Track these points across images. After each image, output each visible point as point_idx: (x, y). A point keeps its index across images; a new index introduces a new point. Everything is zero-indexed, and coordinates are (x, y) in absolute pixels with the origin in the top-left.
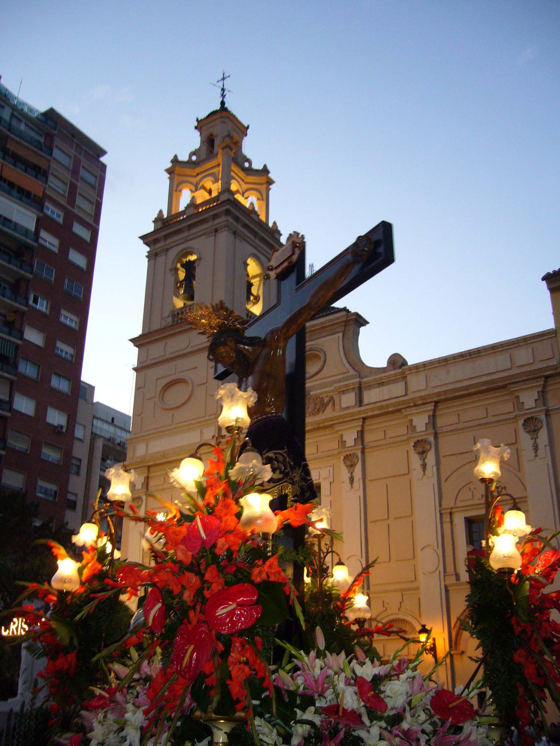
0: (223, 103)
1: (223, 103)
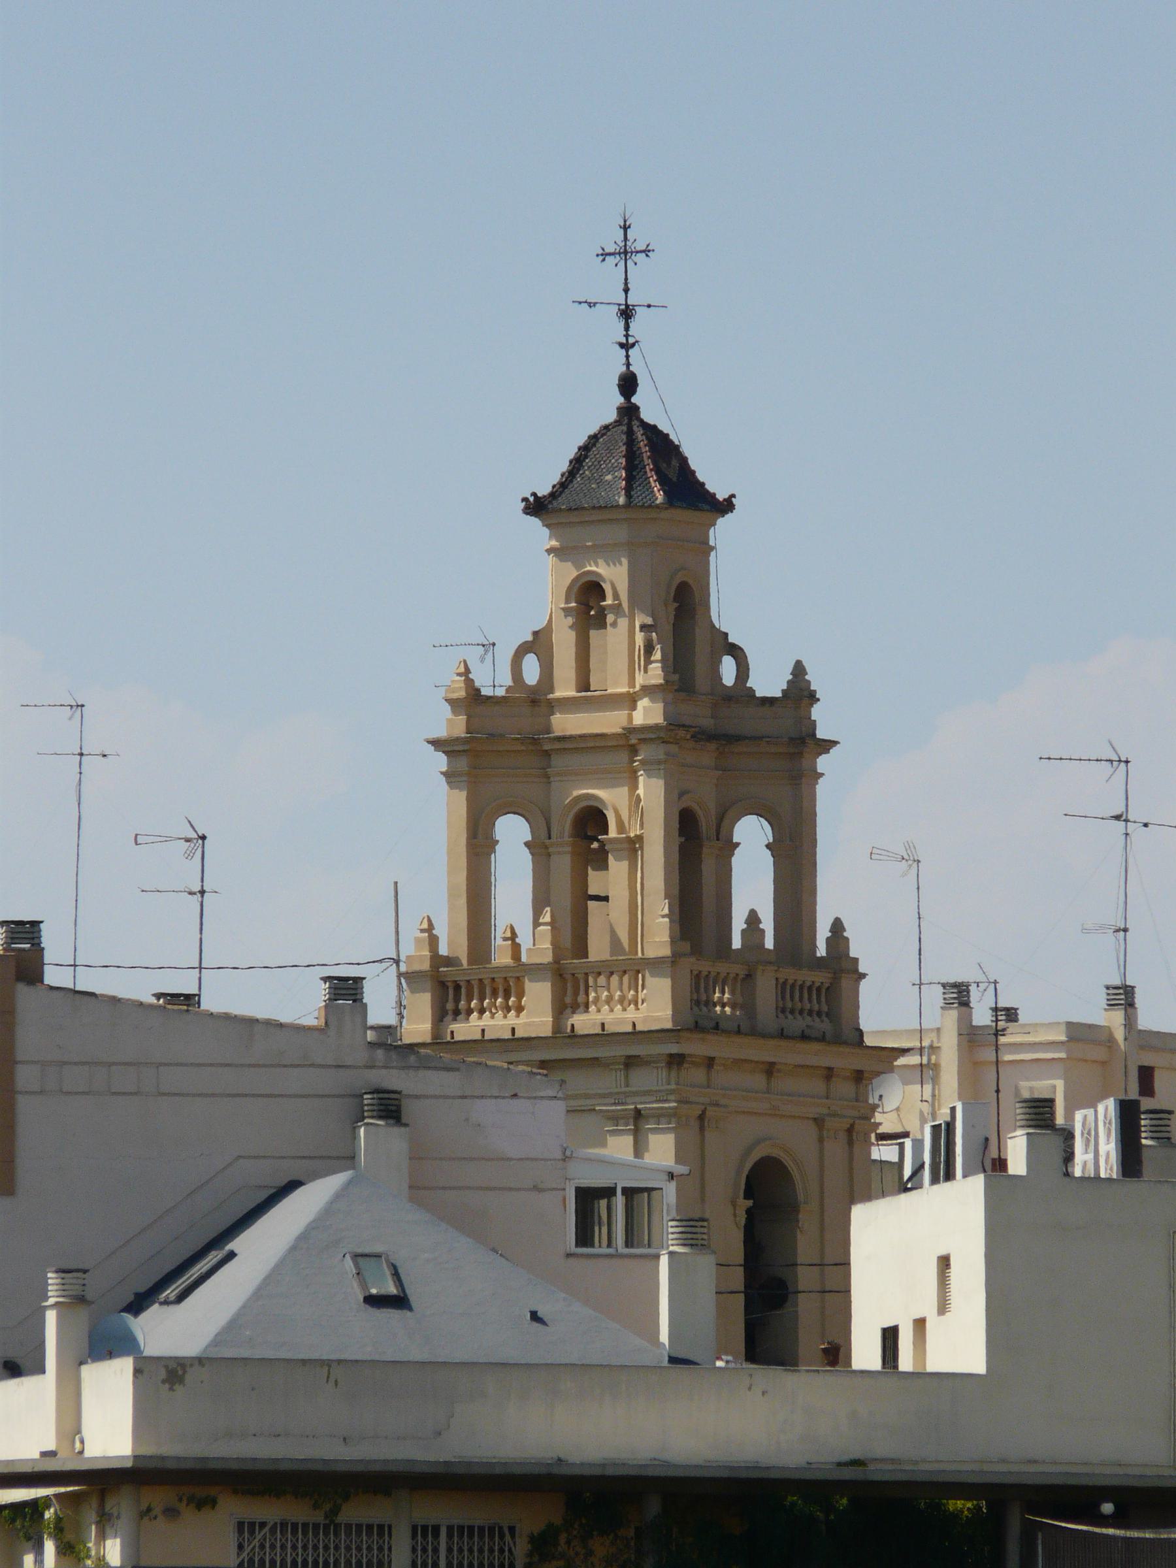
0: (628, 384)
1: (628, 384)
